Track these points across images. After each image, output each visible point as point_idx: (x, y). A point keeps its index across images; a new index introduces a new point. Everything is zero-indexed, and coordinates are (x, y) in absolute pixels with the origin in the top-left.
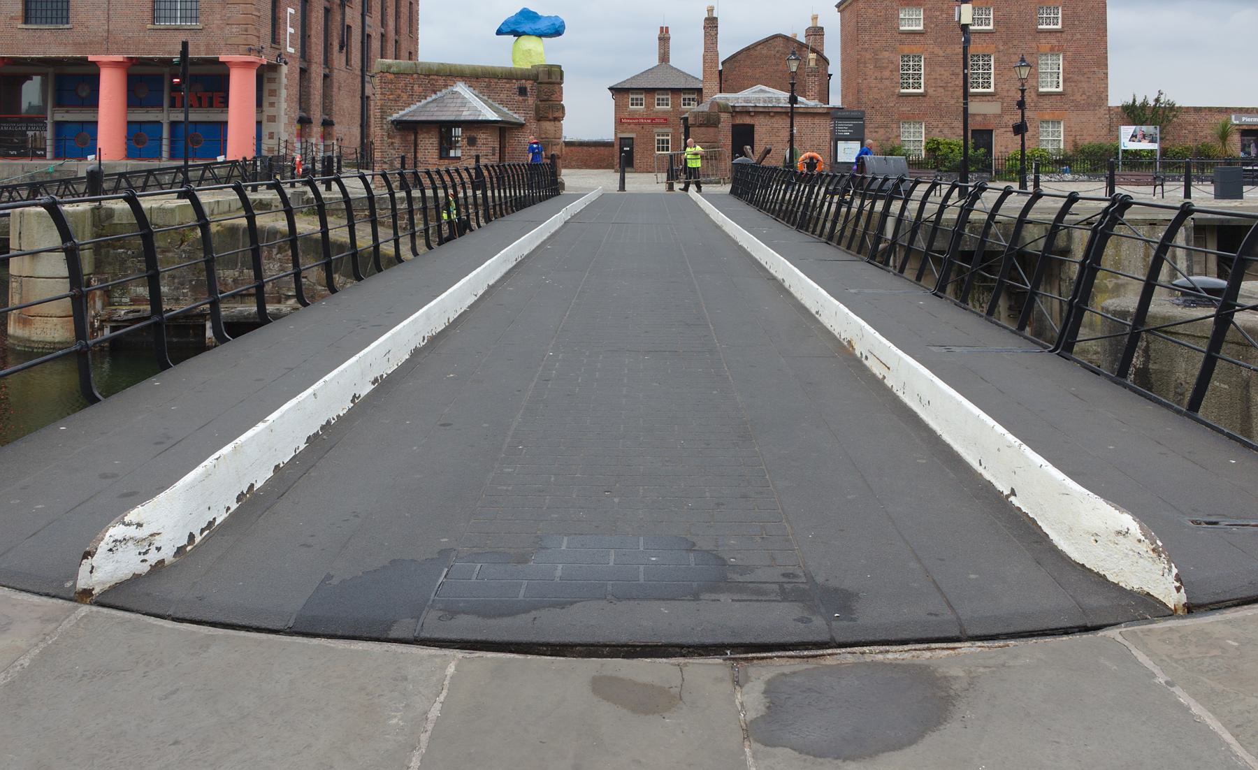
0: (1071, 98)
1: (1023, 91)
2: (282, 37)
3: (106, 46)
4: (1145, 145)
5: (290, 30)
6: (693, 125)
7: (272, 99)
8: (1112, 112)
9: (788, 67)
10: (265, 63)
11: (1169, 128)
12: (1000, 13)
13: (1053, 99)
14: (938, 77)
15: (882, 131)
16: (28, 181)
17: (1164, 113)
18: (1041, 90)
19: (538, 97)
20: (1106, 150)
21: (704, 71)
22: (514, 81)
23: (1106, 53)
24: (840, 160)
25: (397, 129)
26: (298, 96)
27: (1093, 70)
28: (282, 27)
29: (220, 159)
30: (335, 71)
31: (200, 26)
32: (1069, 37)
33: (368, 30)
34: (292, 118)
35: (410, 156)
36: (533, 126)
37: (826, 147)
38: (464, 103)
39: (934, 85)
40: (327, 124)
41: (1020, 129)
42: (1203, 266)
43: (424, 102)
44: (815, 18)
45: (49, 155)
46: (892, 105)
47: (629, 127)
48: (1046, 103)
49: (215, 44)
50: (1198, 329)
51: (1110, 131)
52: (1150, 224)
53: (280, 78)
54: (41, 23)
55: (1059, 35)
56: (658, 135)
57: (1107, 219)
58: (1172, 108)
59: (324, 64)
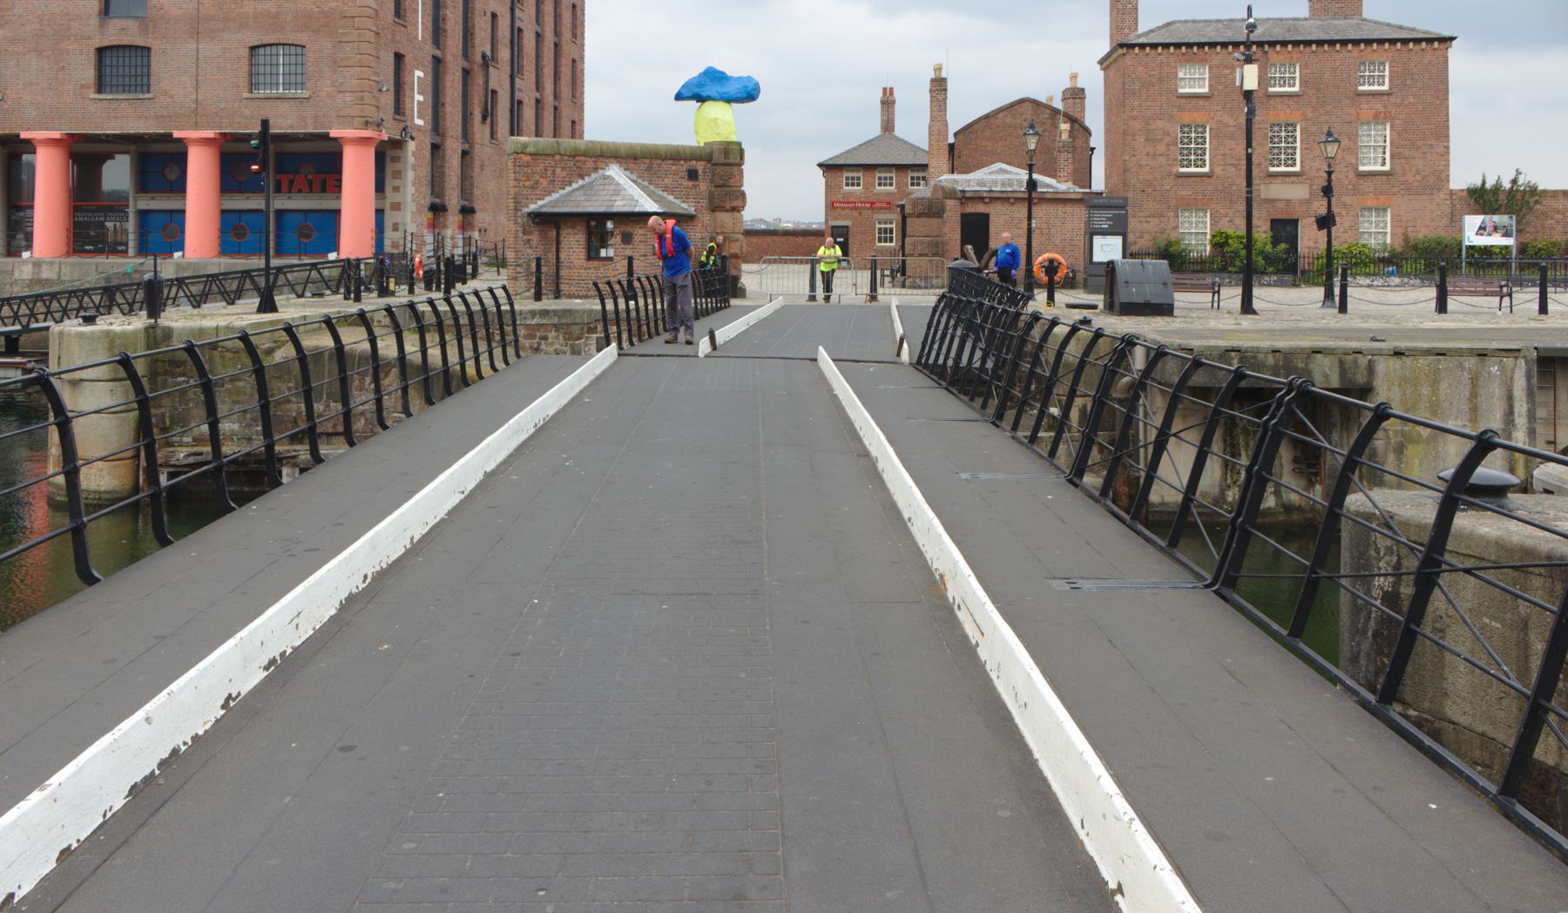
0: (1402, 179)
1: (1329, 173)
2: (408, 106)
3: (194, 120)
4: (1497, 240)
5: (419, 98)
6: (911, 215)
7: (397, 183)
8: (1455, 197)
9: (1025, 144)
10: (386, 139)
11: (1530, 217)
12: (1309, 71)
13: (1377, 179)
14: (1228, 152)
15: (1155, 221)
16: (103, 284)
17: (1523, 197)
18: (1361, 168)
19: (712, 181)
20: (1446, 246)
21: (930, 141)
22: (682, 162)
23: (1448, 121)
24: (1096, 259)
25: (534, 222)
26: (429, 179)
27: (1429, 142)
28: (407, 94)
29: (332, 256)
30: (477, 146)
31: (306, 94)
32: (1399, 101)
33: (518, 95)
34: (422, 206)
35: (552, 256)
36: (706, 217)
37: (1080, 242)
38: (618, 190)
39: (1222, 162)
40: (467, 211)
41: (1326, 222)
42: (1552, 409)
43: (568, 189)
44: (1074, 77)
45: (131, 252)
46: (1168, 188)
47: (843, 213)
48: (1368, 185)
49: (324, 116)
50: (1463, 544)
51: (1452, 220)
52: (1479, 355)
53: (406, 157)
54: (117, 92)
55: (1385, 98)
56: (879, 223)
57: (1281, 412)
58: (1533, 191)
59: (463, 138)
